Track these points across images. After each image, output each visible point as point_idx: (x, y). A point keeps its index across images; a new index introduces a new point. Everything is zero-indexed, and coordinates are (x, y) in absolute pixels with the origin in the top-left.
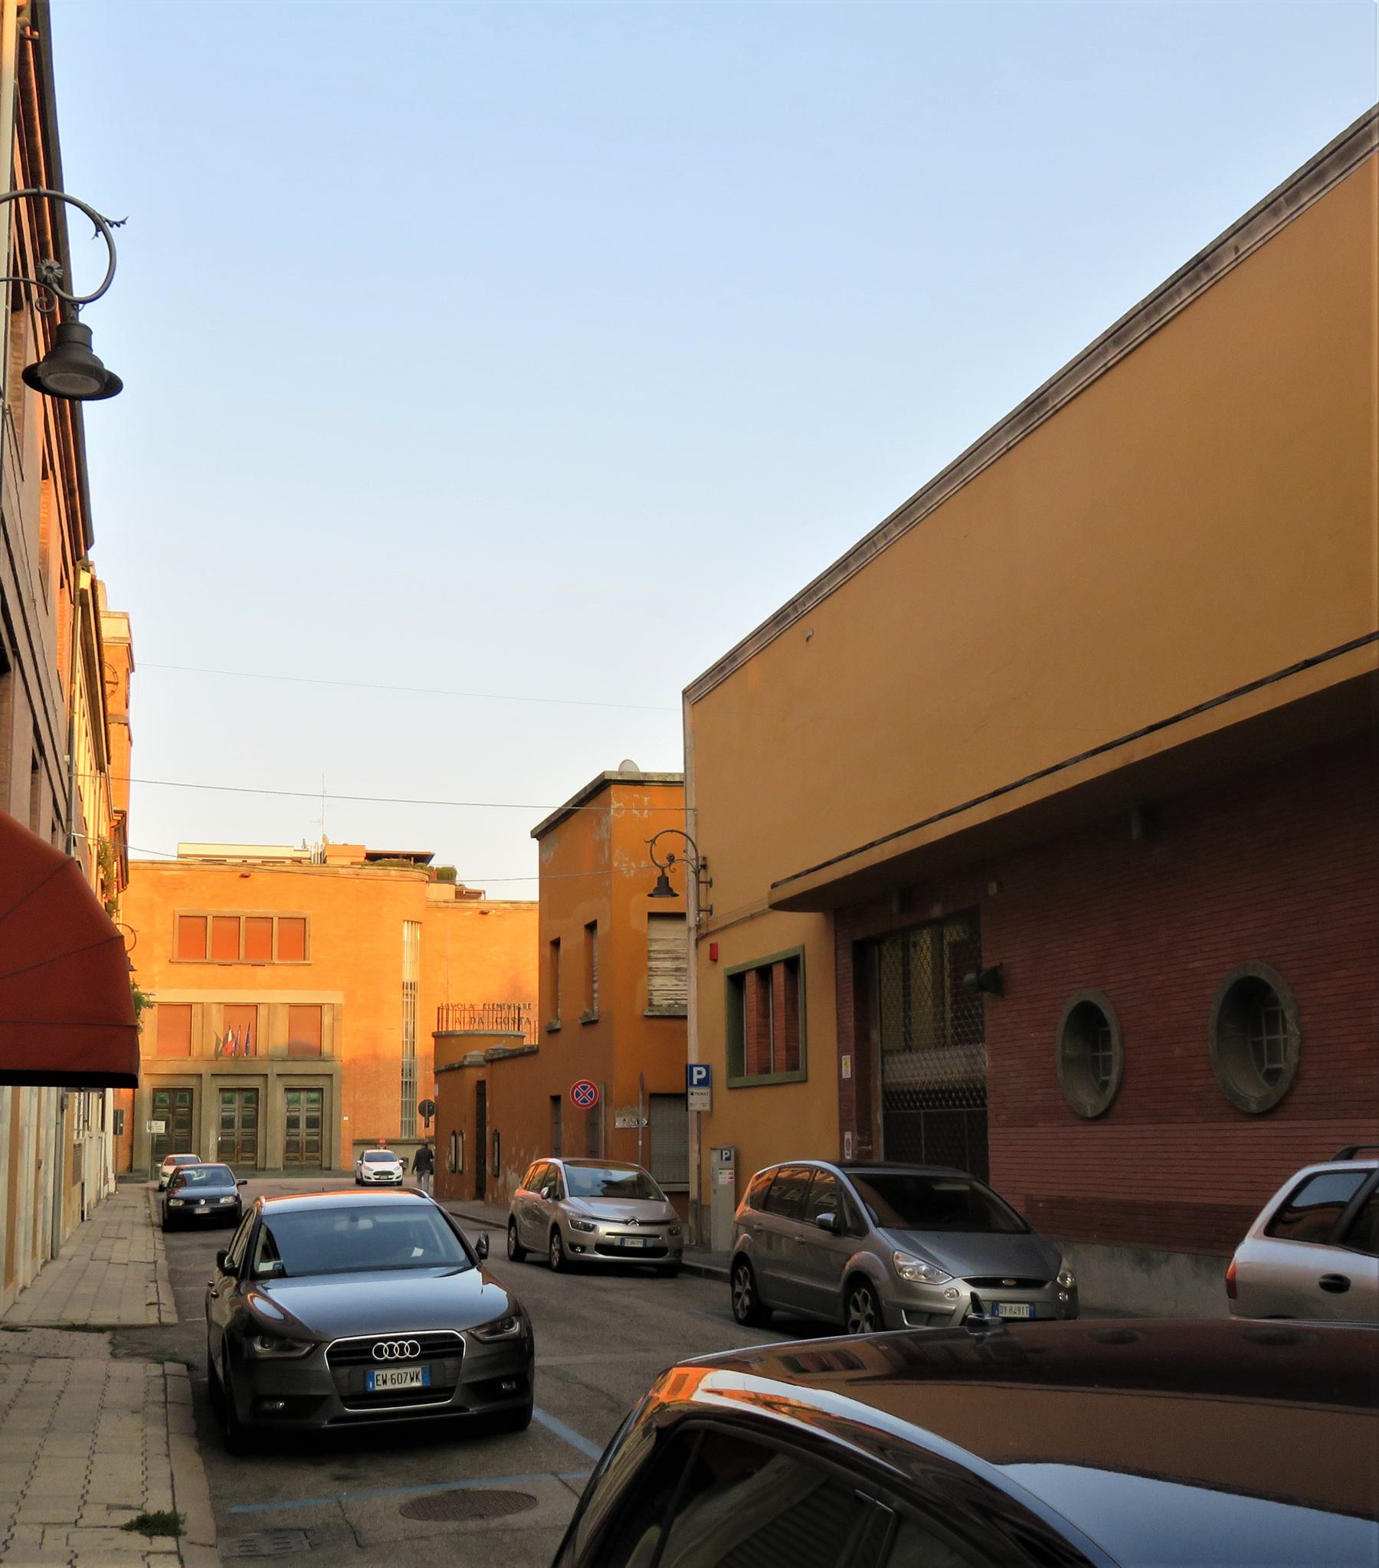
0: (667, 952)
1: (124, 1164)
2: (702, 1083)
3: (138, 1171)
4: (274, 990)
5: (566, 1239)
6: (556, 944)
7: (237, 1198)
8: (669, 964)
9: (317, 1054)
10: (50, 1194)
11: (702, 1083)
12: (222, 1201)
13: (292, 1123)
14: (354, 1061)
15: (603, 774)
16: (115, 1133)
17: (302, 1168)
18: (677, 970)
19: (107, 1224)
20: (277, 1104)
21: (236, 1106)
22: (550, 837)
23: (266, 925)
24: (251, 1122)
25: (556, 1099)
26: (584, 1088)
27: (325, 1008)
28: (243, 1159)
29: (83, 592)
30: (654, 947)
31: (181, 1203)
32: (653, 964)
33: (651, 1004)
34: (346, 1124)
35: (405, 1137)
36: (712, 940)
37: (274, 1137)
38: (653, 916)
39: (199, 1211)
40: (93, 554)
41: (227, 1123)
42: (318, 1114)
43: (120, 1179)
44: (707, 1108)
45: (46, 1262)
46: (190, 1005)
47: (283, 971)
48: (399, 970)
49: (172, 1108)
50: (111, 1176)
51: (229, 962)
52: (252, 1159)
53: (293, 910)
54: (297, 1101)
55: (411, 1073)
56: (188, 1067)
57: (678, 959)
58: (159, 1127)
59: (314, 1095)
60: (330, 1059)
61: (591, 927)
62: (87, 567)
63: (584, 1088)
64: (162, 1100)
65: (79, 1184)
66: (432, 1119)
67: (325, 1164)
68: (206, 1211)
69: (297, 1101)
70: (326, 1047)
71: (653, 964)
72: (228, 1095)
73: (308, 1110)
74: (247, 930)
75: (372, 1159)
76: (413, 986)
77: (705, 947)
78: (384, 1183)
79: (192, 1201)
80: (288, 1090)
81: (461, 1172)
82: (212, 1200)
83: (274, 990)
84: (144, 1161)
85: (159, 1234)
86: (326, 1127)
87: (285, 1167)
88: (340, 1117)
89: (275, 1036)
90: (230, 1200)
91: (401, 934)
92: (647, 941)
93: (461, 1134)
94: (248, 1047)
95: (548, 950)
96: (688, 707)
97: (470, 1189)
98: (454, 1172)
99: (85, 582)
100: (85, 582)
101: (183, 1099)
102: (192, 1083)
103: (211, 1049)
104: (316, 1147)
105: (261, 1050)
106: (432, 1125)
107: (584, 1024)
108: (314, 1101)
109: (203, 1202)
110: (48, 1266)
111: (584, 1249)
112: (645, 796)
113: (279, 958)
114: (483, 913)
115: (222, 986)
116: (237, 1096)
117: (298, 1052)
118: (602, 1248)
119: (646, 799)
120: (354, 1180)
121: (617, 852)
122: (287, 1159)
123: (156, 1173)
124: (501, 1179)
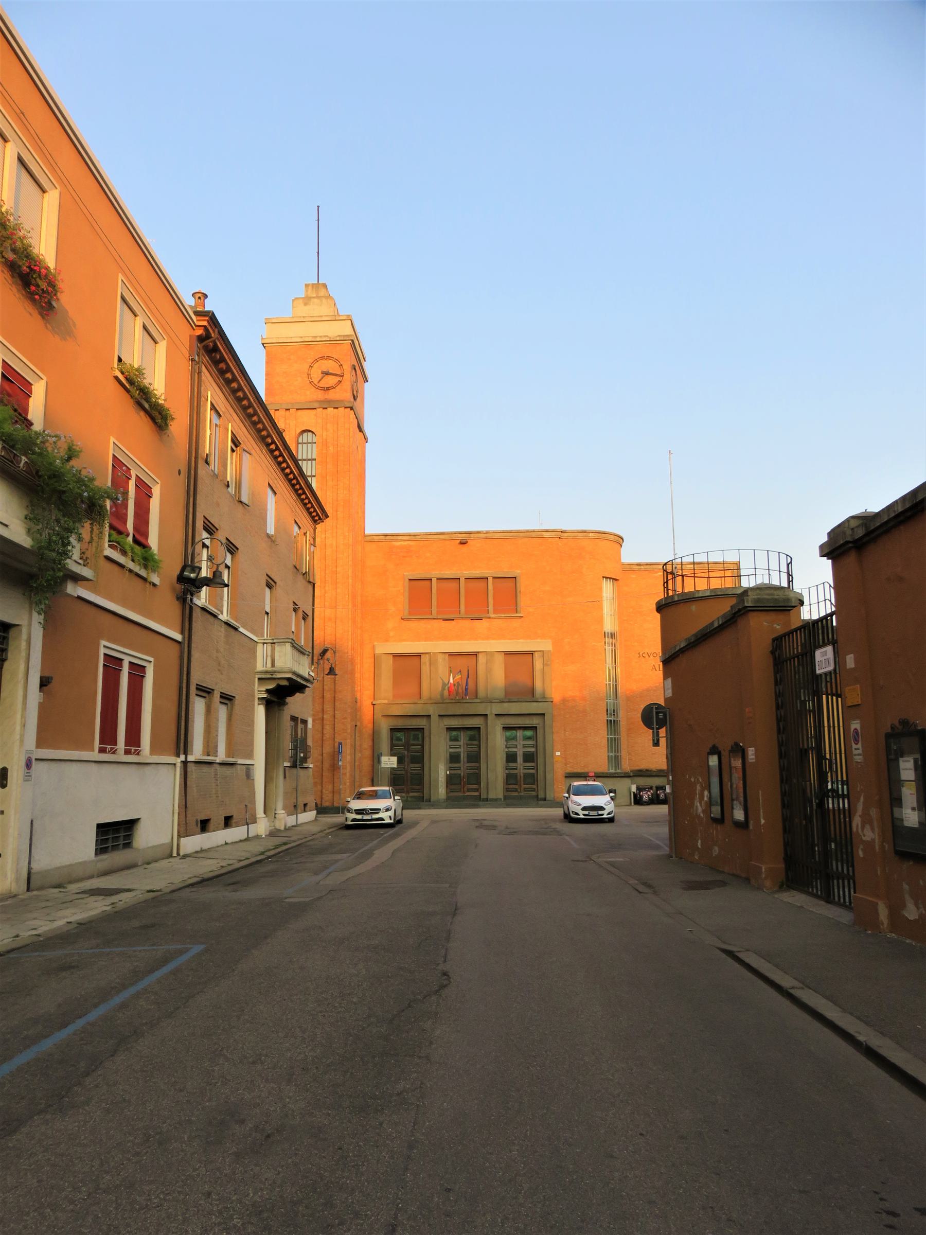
9: (530, 694)
13: (511, 758)
14: (564, 700)
20: (496, 741)
21: (461, 743)
24: (475, 758)
28: (469, 790)
34: (559, 757)
35: (612, 771)
37: (495, 771)
41: (454, 759)
42: (533, 750)
47: (498, 623)
51: (452, 616)
52: (477, 790)
54: (515, 738)
55: (615, 713)
59: (529, 733)
60: (544, 699)
67: (541, 795)
69: (515, 738)
72: (454, 733)
73: (524, 746)
75: (579, 792)
78: (594, 818)
81: (743, 826)
83: (490, 642)
89: (494, 677)
91: (601, 589)
97: (770, 865)
101: (416, 738)
104: (532, 779)
108: (529, 738)
113: (495, 612)
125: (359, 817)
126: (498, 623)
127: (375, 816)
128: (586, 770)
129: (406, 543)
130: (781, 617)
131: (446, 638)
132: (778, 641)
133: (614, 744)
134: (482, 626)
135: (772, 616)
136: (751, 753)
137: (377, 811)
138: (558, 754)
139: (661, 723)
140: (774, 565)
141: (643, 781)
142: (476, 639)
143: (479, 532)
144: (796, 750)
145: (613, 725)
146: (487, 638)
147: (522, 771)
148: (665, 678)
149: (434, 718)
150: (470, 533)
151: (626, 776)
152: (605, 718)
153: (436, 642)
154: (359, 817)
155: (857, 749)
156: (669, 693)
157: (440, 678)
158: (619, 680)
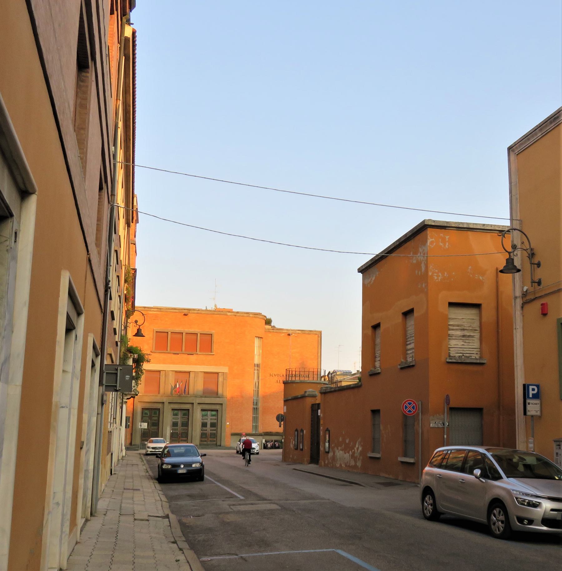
0: (458, 326)
1: (129, 442)
2: (536, 396)
3: (134, 445)
4: (197, 366)
5: (513, 513)
6: (376, 327)
7: (202, 464)
8: (459, 333)
9: (216, 394)
10: (91, 467)
11: (536, 396)
12: (194, 466)
13: (204, 425)
14: (232, 398)
15: (424, 221)
16: (126, 427)
17: (208, 445)
18: (464, 336)
19: (126, 477)
20: (197, 417)
21: (179, 417)
23: (194, 337)
24: (186, 424)
25: (375, 412)
26: (410, 404)
27: (220, 374)
29: (127, 39)
30: (451, 323)
31: (170, 467)
32: (450, 332)
33: (450, 356)
34: (228, 426)
35: (254, 432)
36: (543, 301)
37: (196, 430)
38: (451, 304)
39: (180, 471)
40: (134, 15)
41: (175, 424)
42: (216, 421)
43: (127, 449)
44: (539, 413)
45: (87, 520)
46: (160, 371)
48: (253, 358)
49: (150, 417)
50: (124, 448)
51: (178, 352)
53: (207, 331)
54: (206, 415)
55: (257, 404)
56: (158, 399)
57: (464, 330)
58: (145, 425)
59: (214, 413)
60: (222, 397)
61: (408, 313)
62: (129, 23)
63: (410, 404)
64: (146, 414)
65: (110, 454)
66: (282, 423)
67: (218, 444)
68: (184, 471)
69: (206, 415)
70: (220, 391)
71: (450, 332)
72: (176, 412)
76: (258, 366)
77: (537, 306)
79: (176, 466)
80: (202, 410)
81: (302, 450)
83: (197, 366)
84: (137, 440)
85: (158, 485)
86: (219, 426)
87: (200, 445)
88: (225, 423)
89: (197, 386)
90: (198, 465)
91: (254, 343)
94: (186, 390)
95: (370, 331)
96: (513, 156)
97: (307, 458)
98: (297, 449)
99: (128, 32)
100: (128, 32)
101: (155, 413)
102: (159, 406)
104: (214, 436)
105: (191, 392)
106: (282, 426)
107: (402, 368)
108: (214, 415)
109: (182, 466)
110: (88, 524)
111: (531, 522)
112: (447, 235)
113: (200, 351)
114: (289, 335)
116: (180, 412)
117: (207, 393)
118: (546, 521)
119: (447, 237)
120: (235, 451)
121: (431, 267)
122: (201, 441)
123: (144, 446)
124: (331, 454)
125: (154, 450)
128: (241, 432)
133: (255, 419)
134: (193, 358)
136: (305, 431)
138: (228, 423)
141: (268, 438)
143: (194, 310)
145: (255, 410)
146: (196, 364)
147: (210, 432)
149: (166, 404)
154: (154, 450)
156: (285, 411)
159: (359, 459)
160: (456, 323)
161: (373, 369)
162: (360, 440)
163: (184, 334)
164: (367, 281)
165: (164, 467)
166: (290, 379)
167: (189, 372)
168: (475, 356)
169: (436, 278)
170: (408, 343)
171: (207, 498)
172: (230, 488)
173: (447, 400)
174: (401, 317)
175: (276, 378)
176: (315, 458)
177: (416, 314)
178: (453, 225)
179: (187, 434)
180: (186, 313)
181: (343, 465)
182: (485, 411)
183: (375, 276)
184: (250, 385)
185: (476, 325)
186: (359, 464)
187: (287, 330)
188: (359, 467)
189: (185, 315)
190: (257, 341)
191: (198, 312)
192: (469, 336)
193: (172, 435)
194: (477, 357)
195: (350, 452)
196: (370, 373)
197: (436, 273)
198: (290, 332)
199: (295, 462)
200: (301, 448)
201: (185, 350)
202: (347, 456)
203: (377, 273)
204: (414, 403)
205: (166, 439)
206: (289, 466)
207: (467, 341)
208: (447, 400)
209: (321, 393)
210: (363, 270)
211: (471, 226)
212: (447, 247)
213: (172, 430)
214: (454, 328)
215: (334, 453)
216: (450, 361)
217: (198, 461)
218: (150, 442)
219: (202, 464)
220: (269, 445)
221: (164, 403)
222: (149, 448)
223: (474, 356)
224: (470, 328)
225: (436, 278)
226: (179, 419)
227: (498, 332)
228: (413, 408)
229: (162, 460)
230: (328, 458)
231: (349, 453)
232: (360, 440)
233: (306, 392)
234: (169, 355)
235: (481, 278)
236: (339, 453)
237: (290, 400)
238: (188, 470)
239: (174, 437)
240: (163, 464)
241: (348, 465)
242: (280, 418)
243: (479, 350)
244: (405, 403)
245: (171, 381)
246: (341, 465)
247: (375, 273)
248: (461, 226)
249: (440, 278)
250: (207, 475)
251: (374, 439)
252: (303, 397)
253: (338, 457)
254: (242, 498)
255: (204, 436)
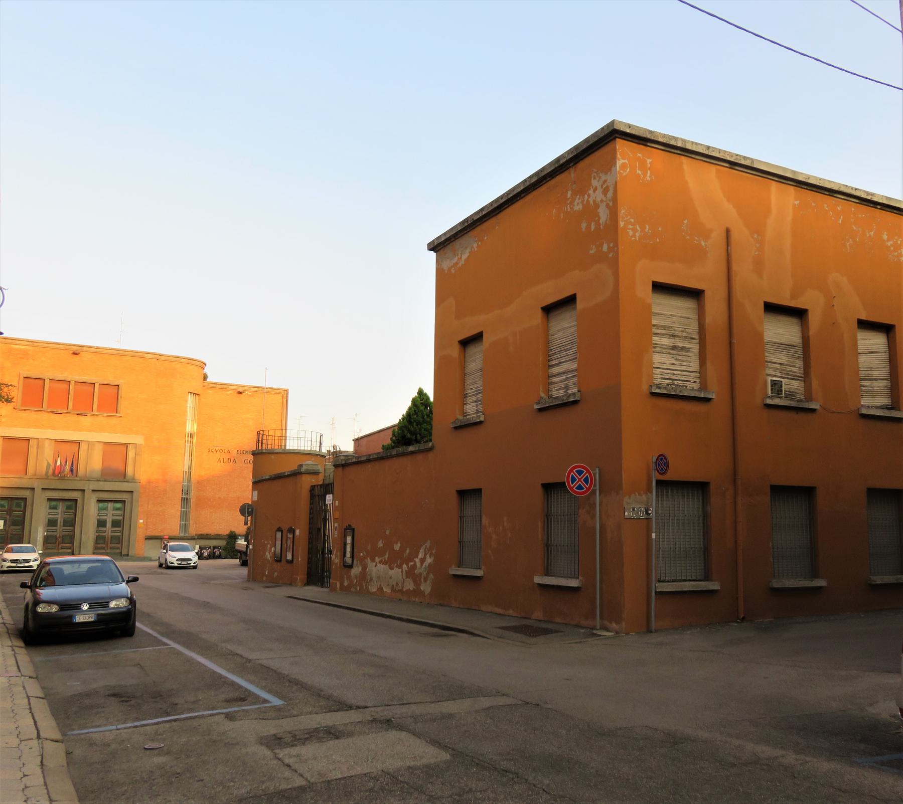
0: (665, 328)
7: (132, 601)
9: (123, 476)
12: (113, 604)
13: (101, 523)
14: (149, 482)
15: (613, 122)
18: (674, 348)
20: (91, 511)
21: (59, 511)
22: (448, 250)
23: (90, 388)
24: (70, 523)
26: (580, 473)
27: (130, 447)
28: (62, 548)
30: (654, 322)
34: (141, 525)
35: (182, 535)
37: (88, 531)
38: (659, 287)
39: (80, 618)
41: (52, 523)
42: (121, 518)
46: (28, 440)
47: (101, 420)
48: (184, 424)
49: (10, 511)
51: (60, 411)
52: (70, 548)
54: (106, 509)
55: (188, 492)
56: (25, 483)
57: (674, 336)
59: (119, 505)
60: (133, 480)
63: (580, 473)
66: (249, 518)
67: (124, 552)
68: (90, 618)
69: (106, 509)
72: (54, 503)
73: (113, 515)
74: (75, 392)
75: (173, 549)
76: (191, 436)
78: (184, 566)
80: (99, 501)
81: (291, 562)
82: (98, 603)
83: (93, 435)
85: (23, 655)
88: (137, 522)
89: (93, 463)
90: (123, 603)
91: (186, 401)
92: (648, 313)
93: (292, 531)
95: (455, 351)
97: (301, 576)
101: (18, 505)
103: (43, 469)
104: (118, 540)
105: (81, 471)
107: (456, 428)
108: (118, 509)
109: (85, 607)
112: (653, 158)
113: (99, 409)
114: (240, 393)
115: (54, 428)
116: (61, 504)
117: (107, 474)
119: (649, 161)
120: (157, 563)
121: (622, 212)
124: (356, 571)
125: (14, 565)
126: (101, 420)
127: (26, 564)
128: (162, 534)
129: (23, 347)
130: (315, 476)
131: (54, 428)
132: (313, 488)
133: (185, 515)
134: (86, 421)
135: (312, 476)
136: (297, 532)
137: (28, 561)
138: (141, 521)
139: (250, 514)
140: (314, 440)
141: (204, 543)
142: (80, 431)
143: (90, 347)
144: (316, 532)
145: (185, 501)
146: (90, 431)
147: (110, 534)
148: (253, 490)
149: (38, 491)
150: (83, 346)
151: (192, 539)
152: (180, 496)
153: (47, 431)
154: (14, 565)
155: (336, 533)
156: (255, 498)
157: (43, 460)
158: (193, 468)
159: (425, 580)
160: (662, 323)
161: (460, 417)
162: (428, 544)
163: (72, 383)
164: (446, 265)
165: (39, 610)
166: (264, 447)
167: (79, 443)
168: (692, 387)
169: (631, 233)
170: (554, 363)
171: (175, 708)
172: (210, 658)
173: (662, 463)
174: (539, 314)
175: (218, 455)
176: (317, 573)
177: (580, 304)
178: (661, 140)
179: (71, 538)
180: (76, 352)
181: (387, 590)
182: (712, 487)
183: (468, 251)
184: (184, 462)
185: (693, 328)
186: (426, 588)
187: (237, 386)
188: (427, 592)
189: (75, 354)
190: (190, 399)
191: (98, 352)
192: (683, 348)
193: (46, 540)
194: (696, 386)
195: (405, 566)
196: (356, 451)
197: (631, 224)
198: (240, 389)
199: (274, 582)
200: (289, 557)
201: (74, 408)
202: (396, 574)
203: (475, 245)
204: (588, 471)
205: (35, 544)
206: (267, 590)
207: (680, 358)
208: (662, 463)
209: (336, 466)
210: (436, 247)
211: (689, 147)
212: (648, 178)
213: (48, 531)
214: (659, 331)
215: (365, 567)
216: (658, 391)
217: (125, 594)
218: (7, 552)
219: (132, 601)
220: (205, 554)
221: (33, 489)
222: (4, 560)
223: (691, 385)
224: (684, 334)
225: (631, 233)
226: (60, 514)
227: (731, 344)
228: (586, 480)
229: (35, 594)
230: (349, 577)
231: (400, 567)
232: (428, 544)
233: (301, 466)
234: (46, 415)
235: (703, 244)
236: (377, 568)
237: (266, 480)
238: (98, 615)
239: (51, 544)
240: (37, 602)
241: (398, 588)
242: (246, 510)
243: (698, 375)
244: (571, 471)
245: (48, 453)
246: (380, 589)
247: (464, 252)
248: (672, 143)
249: (637, 234)
250: (142, 622)
251: (460, 542)
252: (296, 474)
253: (374, 574)
254: (276, 701)
255: (101, 541)
